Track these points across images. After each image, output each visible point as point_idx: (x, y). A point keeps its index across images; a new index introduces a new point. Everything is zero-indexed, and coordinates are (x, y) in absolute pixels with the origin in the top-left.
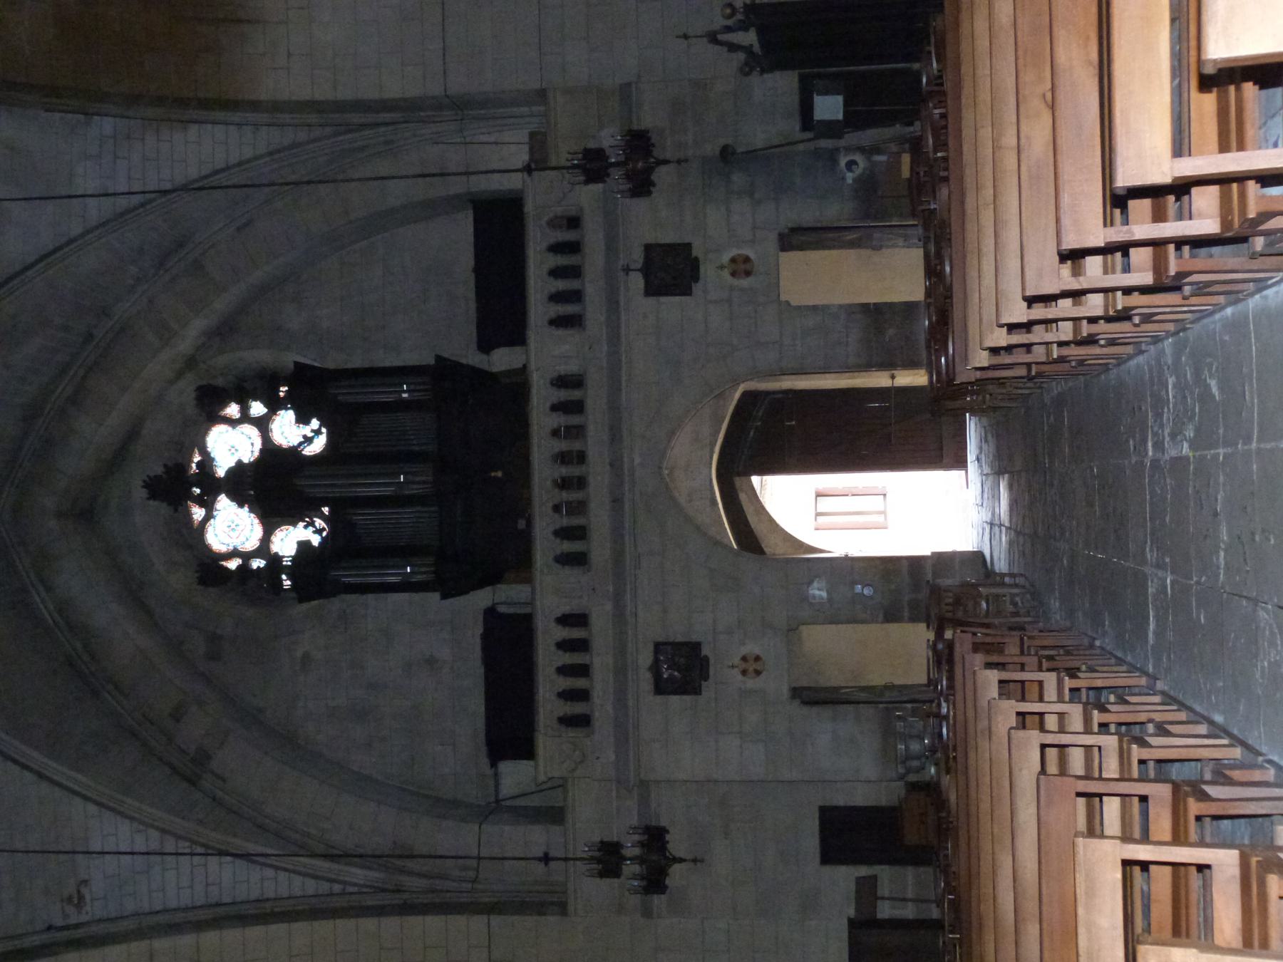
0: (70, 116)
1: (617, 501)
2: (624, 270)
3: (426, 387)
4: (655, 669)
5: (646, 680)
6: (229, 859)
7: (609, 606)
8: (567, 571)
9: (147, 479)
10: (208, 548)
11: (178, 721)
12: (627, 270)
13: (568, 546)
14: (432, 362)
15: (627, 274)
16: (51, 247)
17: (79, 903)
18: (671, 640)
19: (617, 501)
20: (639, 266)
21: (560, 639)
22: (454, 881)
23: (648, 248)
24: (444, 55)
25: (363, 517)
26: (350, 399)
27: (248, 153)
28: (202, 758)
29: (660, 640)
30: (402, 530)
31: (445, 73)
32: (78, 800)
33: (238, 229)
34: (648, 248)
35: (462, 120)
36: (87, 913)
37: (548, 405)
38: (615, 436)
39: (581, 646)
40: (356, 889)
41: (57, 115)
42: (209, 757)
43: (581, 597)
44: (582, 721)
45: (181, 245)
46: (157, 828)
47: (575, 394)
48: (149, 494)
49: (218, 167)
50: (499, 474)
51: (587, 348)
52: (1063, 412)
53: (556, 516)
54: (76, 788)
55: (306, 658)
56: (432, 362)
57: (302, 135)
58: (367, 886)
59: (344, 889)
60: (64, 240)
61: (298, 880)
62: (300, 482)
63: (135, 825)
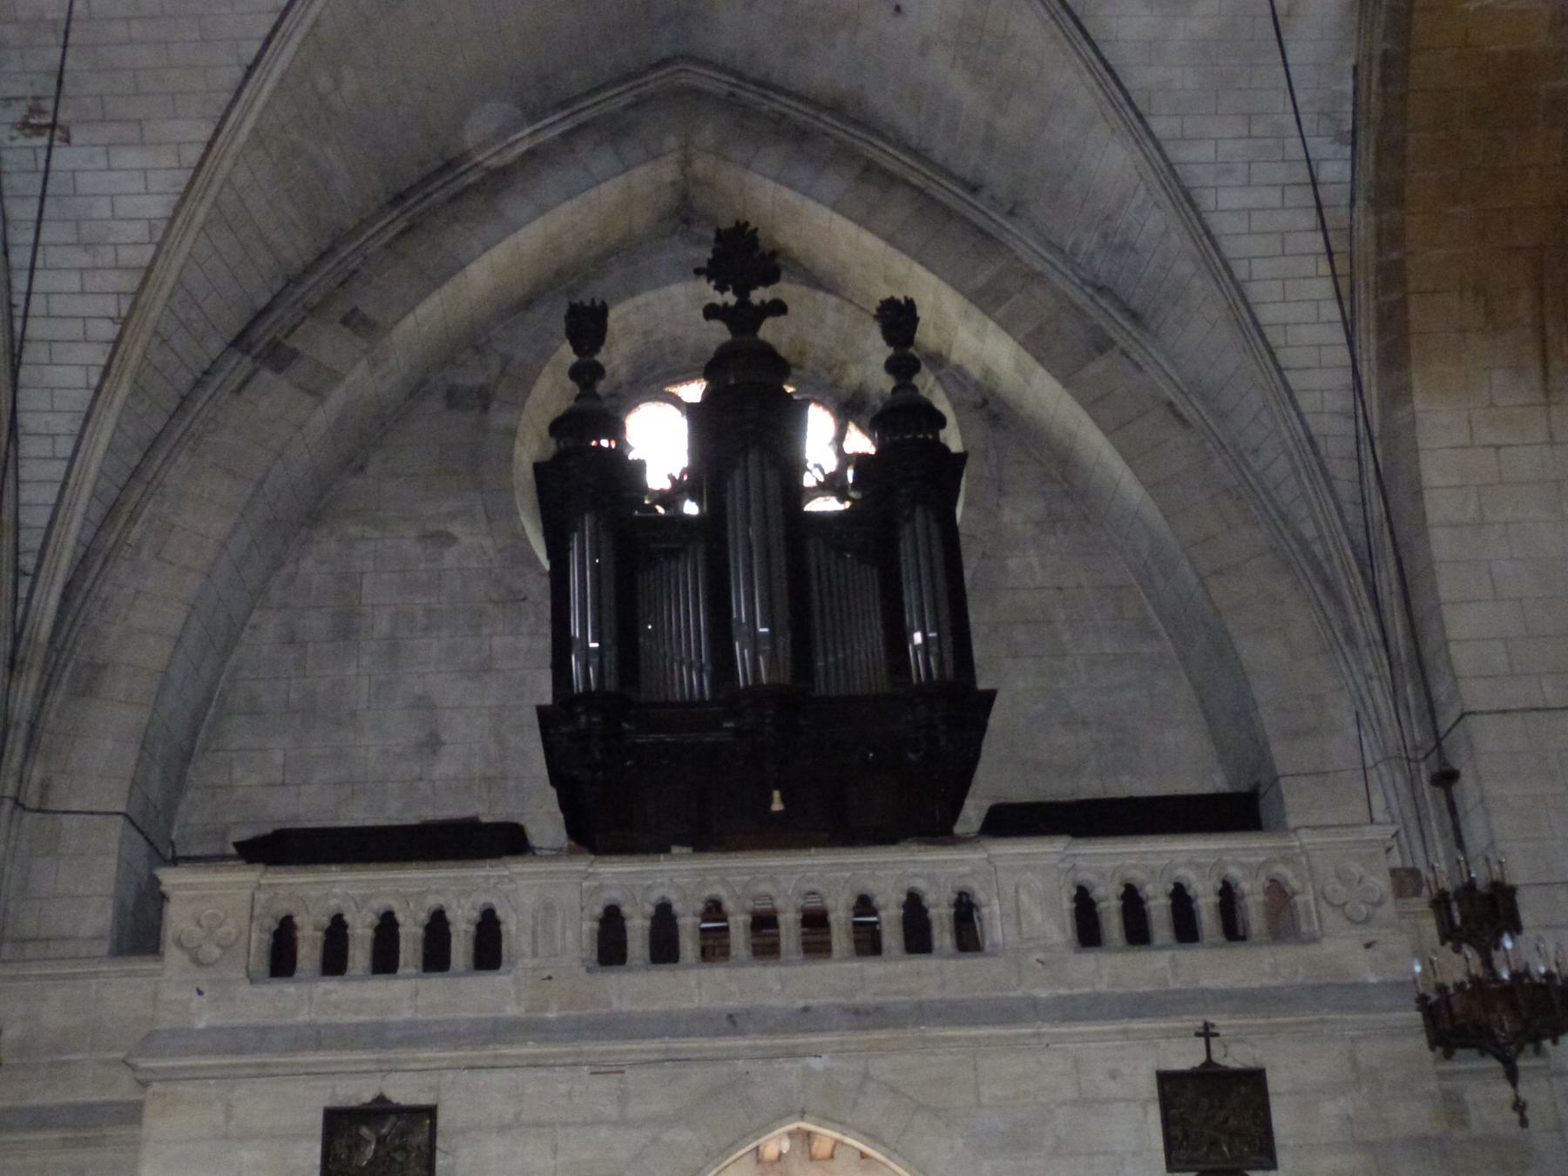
0: (1349, 107)
1: (733, 1022)
2: (1206, 1026)
3: (934, 671)
4: (379, 1110)
5: (357, 1092)
6: (95, 381)
7: (512, 1010)
8: (590, 926)
9: (752, 227)
10: (631, 406)
11: (345, 321)
12: (1207, 1033)
13: (637, 928)
14: (982, 685)
15: (1198, 1035)
16: (1127, 85)
17: (32, 126)
18: (440, 1143)
19: (733, 1022)
20: (1217, 1057)
21: (449, 915)
22: (22, 766)
23: (1255, 1079)
24: (1537, 709)
25: (689, 577)
26: (905, 547)
27: (1307, 402)
28: (278, 357)
29: (442, 1121)
30: (665, 600)
31: (1505, 712)
32: (206, 131)
33: (1170, 405)
34: (1255, 1079)
35: (1407, 758)
36: (12, 139)
37: (920, 884)
38: (863, 1016)
39: (436, 957)
40: (23, 593)
41: (1348, 86)
42: (278, 369)
43: (535, 954)
44: (282, 961)
45: (1134, 316)
46: (154, 259)
47: (943, 936)
48: (726, 231)
49: (1280, 355)
50: (777, 806)
51: (1041, 956)
52: (370, 1163)
53: (700, 906)
54: (229, 125)
55: (448, 539)
56: (982, 685)
57: (1346, 490)
58: (26, 614)
59: (26, 574)
60: (1142, 108)
61: (49, 494)
62: (753, 458)
63: (163, 225)
